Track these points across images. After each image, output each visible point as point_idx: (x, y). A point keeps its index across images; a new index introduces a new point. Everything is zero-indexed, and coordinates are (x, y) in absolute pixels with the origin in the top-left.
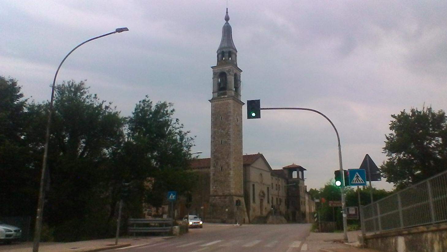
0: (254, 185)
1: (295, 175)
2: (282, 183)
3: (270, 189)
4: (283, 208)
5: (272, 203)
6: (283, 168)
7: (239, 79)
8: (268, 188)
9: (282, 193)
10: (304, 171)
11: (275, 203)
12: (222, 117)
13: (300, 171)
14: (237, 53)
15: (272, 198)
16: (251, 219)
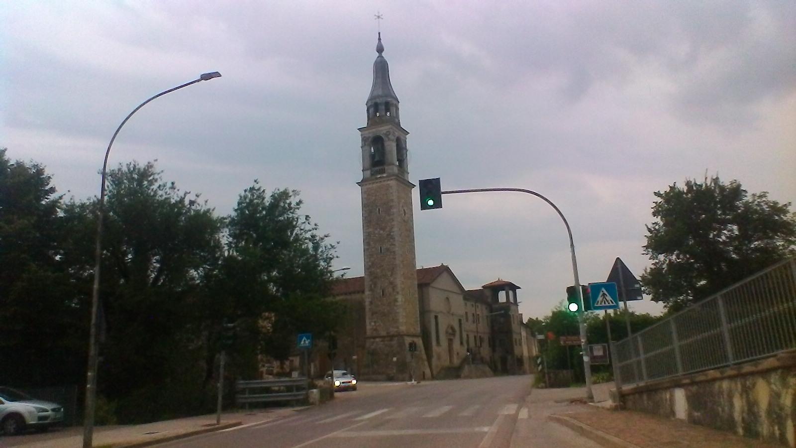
0: (436, 317)
4: (485, 351)
8: (460, 320)
9: (483, 328)
11: (472, 344)
15: (467, 335)
16: (435, 373)
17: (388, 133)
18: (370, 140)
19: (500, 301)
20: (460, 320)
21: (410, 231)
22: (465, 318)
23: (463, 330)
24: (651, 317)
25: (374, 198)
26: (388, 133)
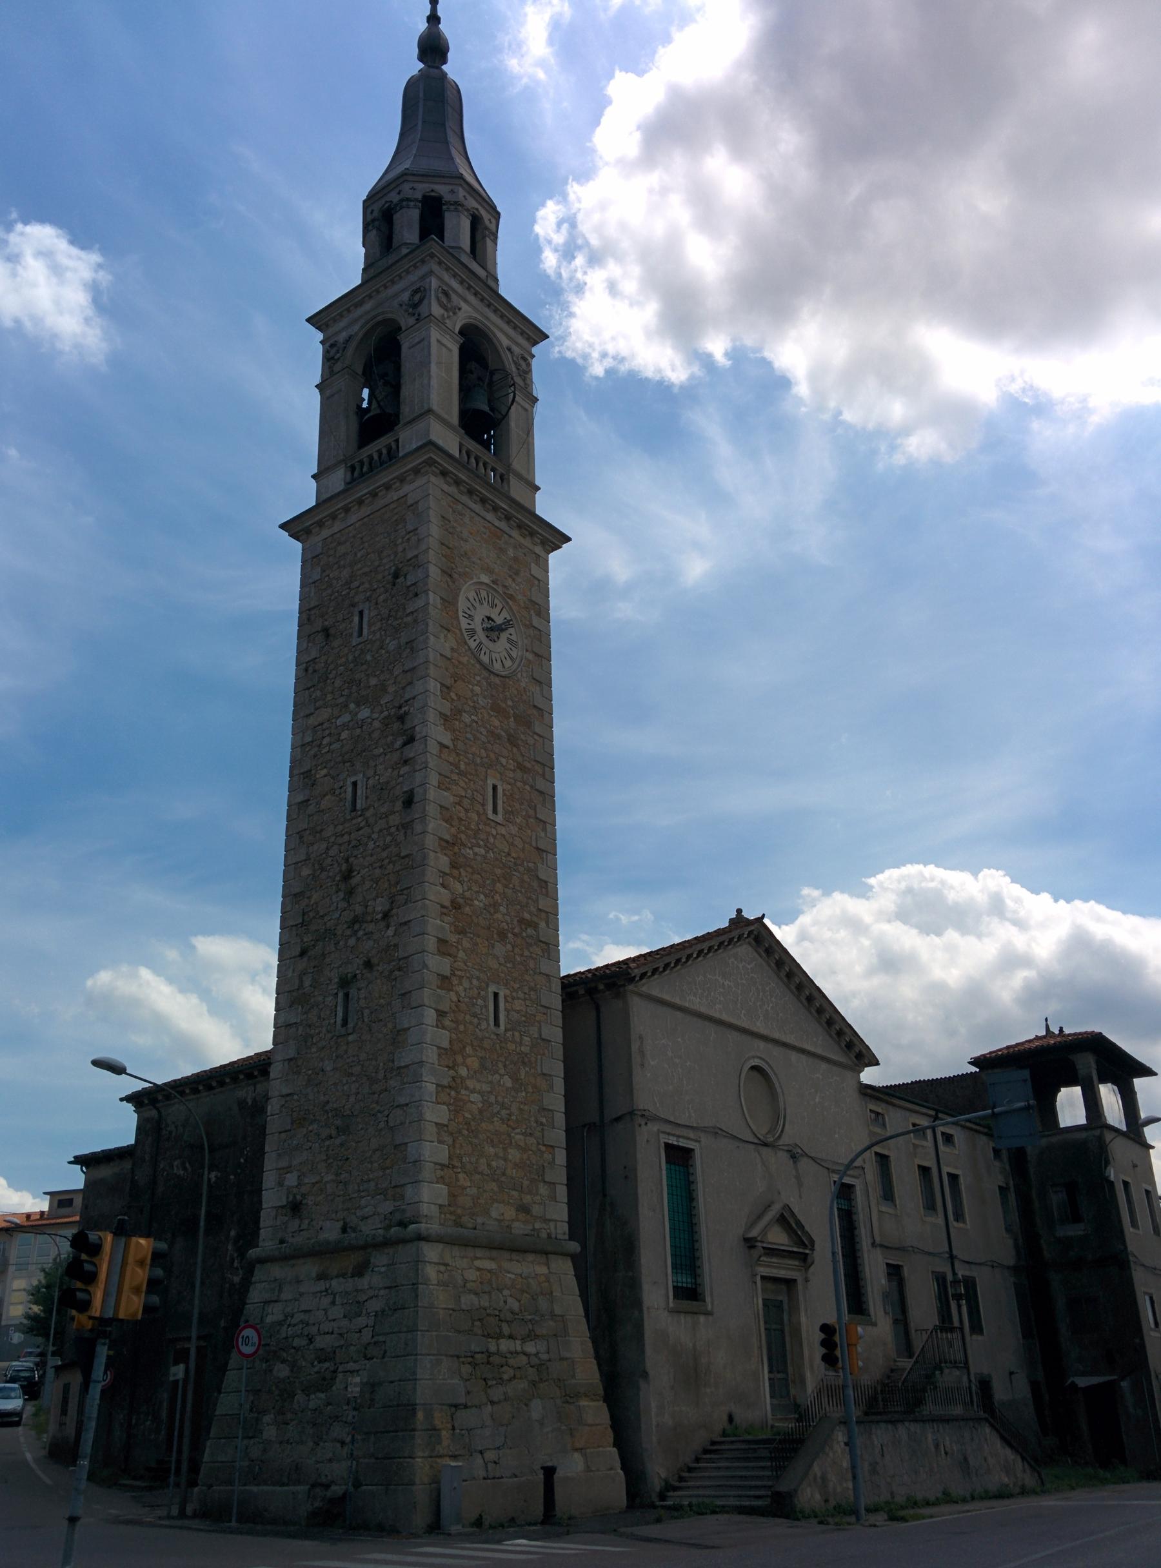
0: (679, 1157)
1: (1070, 1107)
2: (965, 1155)
3: (866, 1185)
4: (996, 1351)
5: (902, 1321)
6: (975, 1062)
7: (373, 233)
8: (845, 1192)
9: (984, 1236)
10: (1139, 1083)
11: (923, 1310)
12: (501, 995)
13: (1103, 1081)
14: (539, 405)
15: (894, 1272)
16: (658, 1470)
17: (417, 298)
18: (353, 344)
19: (1062, 1125)
20: (845, 1192)
21: (525, 722)
22: (871, 1173)
23: (865, 1243)
24: (28, 1190)
25: (345, 573)
26: (417, 298)
